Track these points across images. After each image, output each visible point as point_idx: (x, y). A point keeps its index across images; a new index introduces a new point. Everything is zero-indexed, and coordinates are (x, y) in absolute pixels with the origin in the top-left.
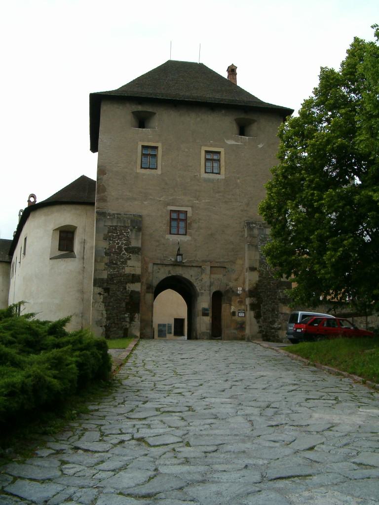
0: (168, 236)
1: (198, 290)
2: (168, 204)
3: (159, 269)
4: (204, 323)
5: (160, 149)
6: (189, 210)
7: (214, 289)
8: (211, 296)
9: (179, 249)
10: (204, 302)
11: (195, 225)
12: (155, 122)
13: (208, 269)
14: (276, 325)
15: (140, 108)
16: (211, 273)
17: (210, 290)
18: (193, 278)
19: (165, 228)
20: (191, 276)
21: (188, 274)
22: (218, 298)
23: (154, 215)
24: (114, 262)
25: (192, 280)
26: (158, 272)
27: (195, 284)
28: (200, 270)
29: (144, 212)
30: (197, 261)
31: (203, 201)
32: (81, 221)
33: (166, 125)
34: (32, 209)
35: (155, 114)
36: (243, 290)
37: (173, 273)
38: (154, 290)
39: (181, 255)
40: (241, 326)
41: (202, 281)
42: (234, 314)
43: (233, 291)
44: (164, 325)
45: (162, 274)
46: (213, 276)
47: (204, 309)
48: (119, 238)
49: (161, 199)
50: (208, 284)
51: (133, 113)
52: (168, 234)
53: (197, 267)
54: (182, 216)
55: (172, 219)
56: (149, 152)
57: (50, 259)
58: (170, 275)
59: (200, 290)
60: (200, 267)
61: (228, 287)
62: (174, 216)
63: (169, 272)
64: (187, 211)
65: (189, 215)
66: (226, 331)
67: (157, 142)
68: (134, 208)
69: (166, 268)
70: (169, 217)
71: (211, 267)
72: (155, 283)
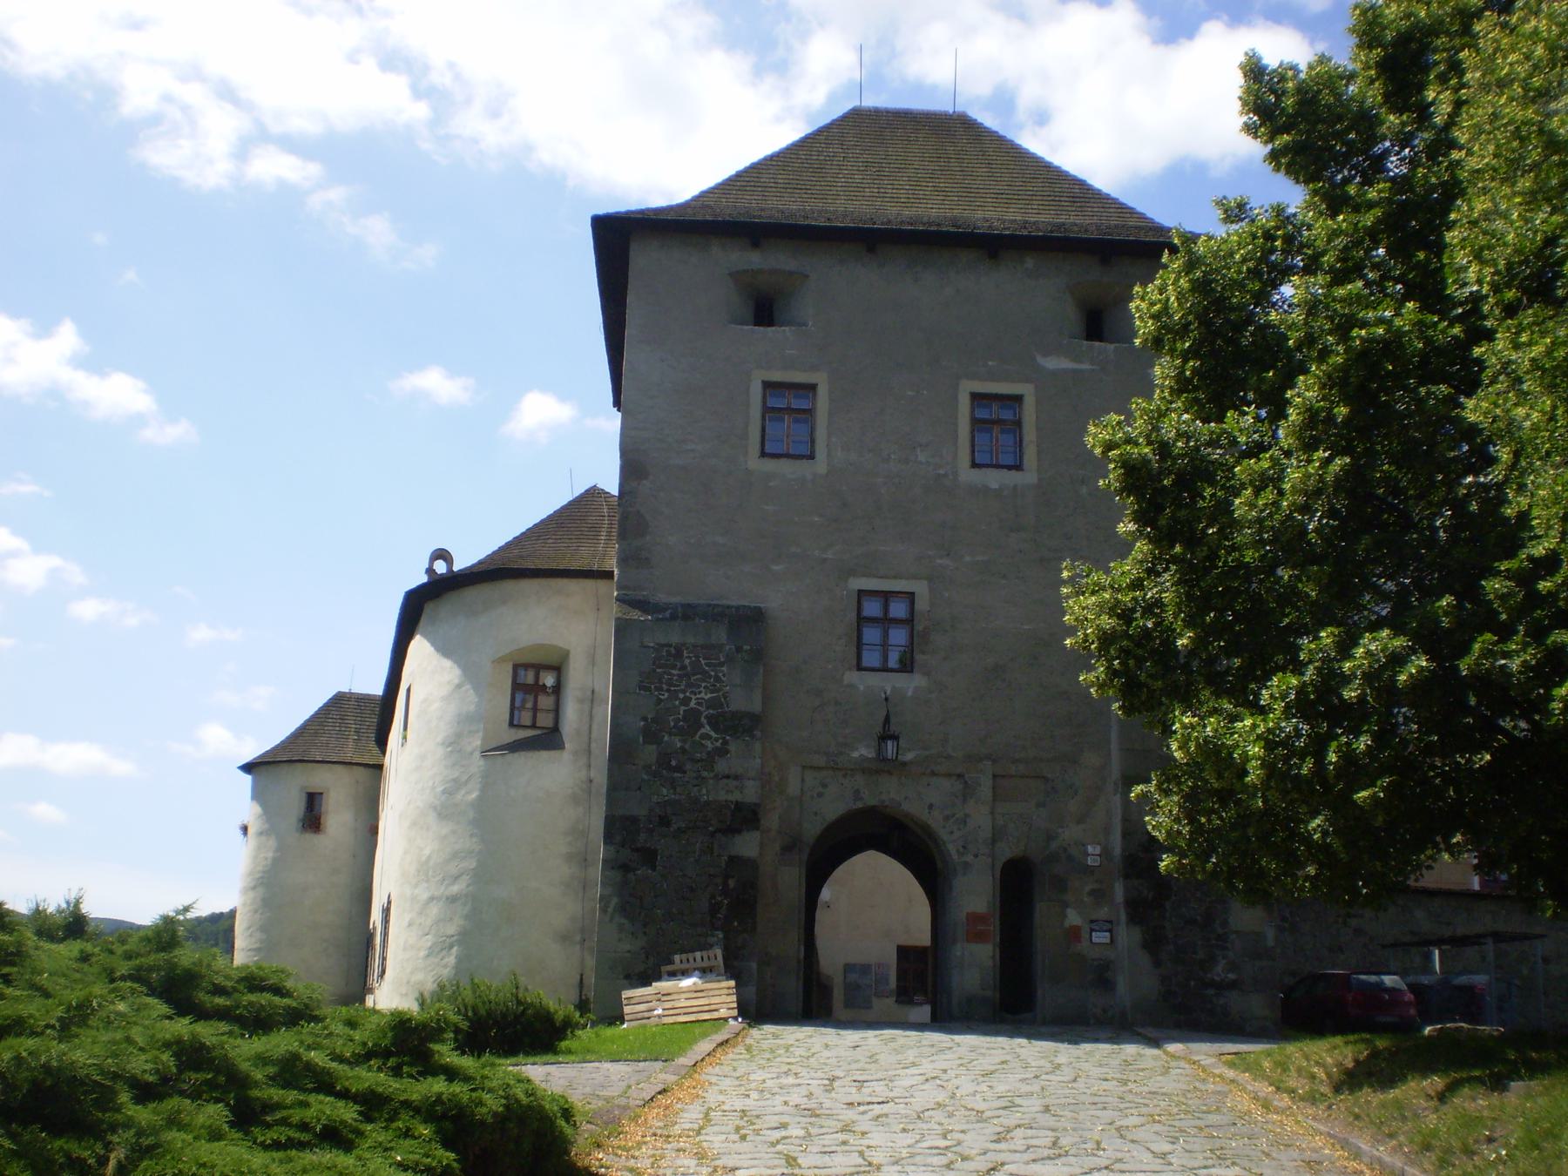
0: (852, 677)
1: (955, 857)
2: (853, 573)
3: (825, 786)
4: (974, 964)
6: (920, 588)
7: (1006, 851)
8: (998, 876)
9: (887, 720)
10: (975, 894)
13: (985, 789)
14: (1219, 971)
15: (754, 259)
21: (919, 800)
22: (1019, 883)
23: (795, 600)
24: (674, 763)
25: (935, 821)
26: (820, 795)
27: (943, 834)
29: (773, 599)
30: (949, 757)
31: (968, 559)
36: (1106, 853)
37: (870, 800)
38: (805, 857)
39: (895, 738)
40: (1102, 976)
42: (1074, 934)
44: (865, 969)
47: (974, 918)
48: (689, 685)
49: (829, 555)
51: (736, 276)
53: (949, 775)
54: (898, 610)
55: (862, 620)
56: (788, 403)
58: (860, 805)
59: (961, 854)
60: (960, 776)
61: (1054, 845)
62: (872, 608)
63: (857, 794)
64: (913, 594)
65: (922, 605)
66: (1047, 995)
68: (733, 586)
70: (854, 614)
71: (994, 776)
72: (812, 829)
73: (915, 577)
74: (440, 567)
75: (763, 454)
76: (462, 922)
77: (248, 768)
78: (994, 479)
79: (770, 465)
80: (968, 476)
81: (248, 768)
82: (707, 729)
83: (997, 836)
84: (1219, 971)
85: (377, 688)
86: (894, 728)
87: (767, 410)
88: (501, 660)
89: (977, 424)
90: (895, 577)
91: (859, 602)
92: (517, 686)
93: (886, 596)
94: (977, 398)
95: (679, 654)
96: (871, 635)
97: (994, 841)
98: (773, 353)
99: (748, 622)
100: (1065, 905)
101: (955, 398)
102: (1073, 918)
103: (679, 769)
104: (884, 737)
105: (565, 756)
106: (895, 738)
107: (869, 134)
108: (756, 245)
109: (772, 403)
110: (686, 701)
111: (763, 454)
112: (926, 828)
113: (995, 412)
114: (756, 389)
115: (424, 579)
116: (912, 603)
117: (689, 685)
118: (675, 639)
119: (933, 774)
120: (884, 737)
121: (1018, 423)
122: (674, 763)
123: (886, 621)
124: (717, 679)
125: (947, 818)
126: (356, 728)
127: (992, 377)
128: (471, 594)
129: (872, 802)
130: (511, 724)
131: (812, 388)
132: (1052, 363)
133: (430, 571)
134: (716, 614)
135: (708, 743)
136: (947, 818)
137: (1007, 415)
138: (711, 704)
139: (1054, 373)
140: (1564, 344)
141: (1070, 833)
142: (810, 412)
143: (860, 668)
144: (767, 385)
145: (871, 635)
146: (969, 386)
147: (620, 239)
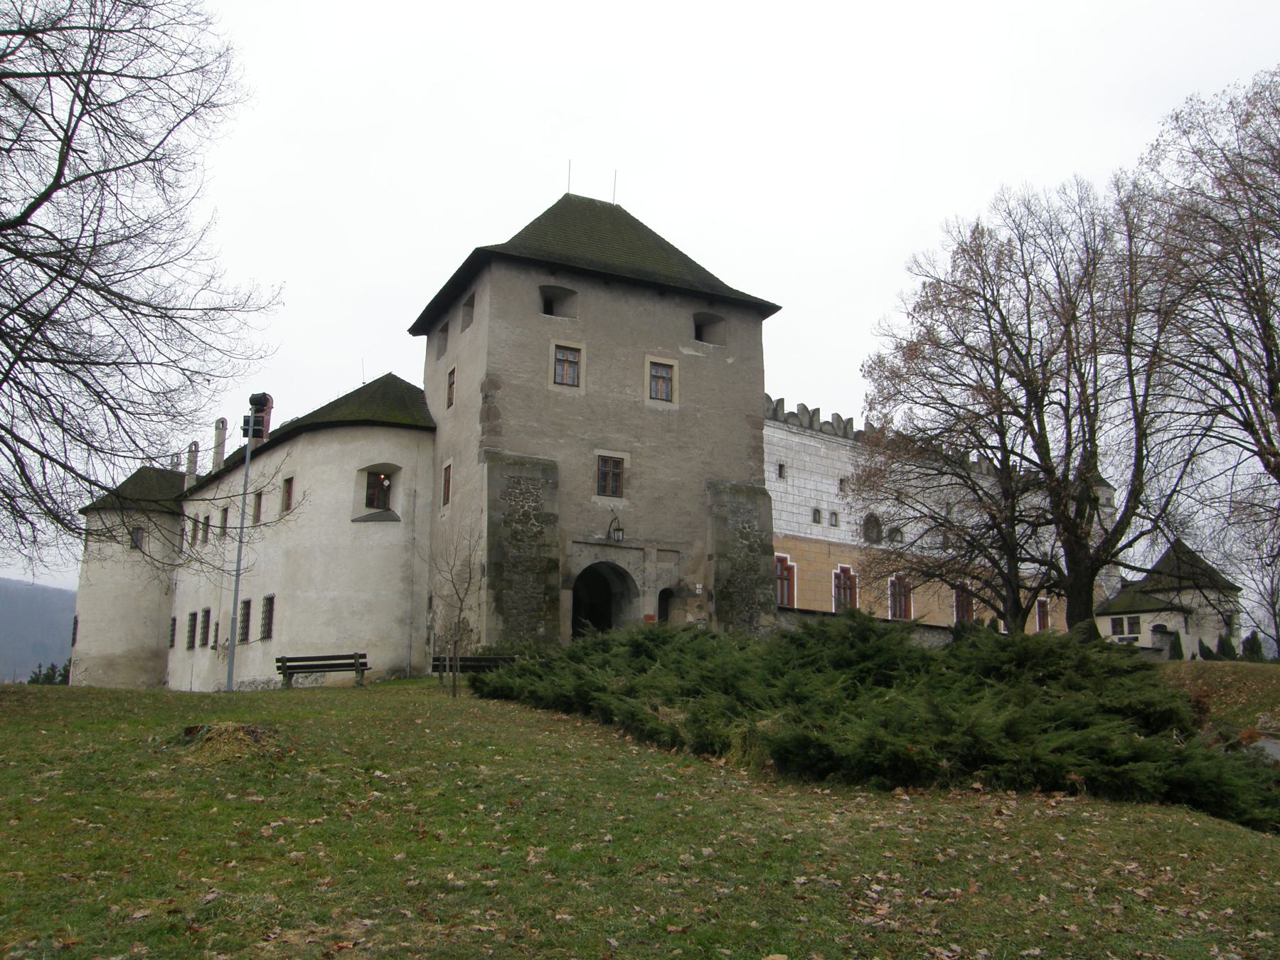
0: (595, 498)
2: (596, 446)
5: (583, 353)
6: (626, 456)
7: (661, 587)
11: (635, 483)
13: (654, 552)
15: (552, 281)
16: (659, 560)
23: (575, 464)
25: (630, 569)
27: (634, 577)
28: (641, 553)
29: (559, 457)
35: (575, 293)
36: (704, 588)
46: (661, 565)
50: (654, 577)
67: (579, 341)
68: (542, 450)
72: (576, 571)
78: (661, 406)
79: (558, 389)
80: (649, 403)
81: (416, 330)
82: (533, 521)
83: (658, 578)
87: (558, 360)
88: (362, 470)
89: (654, 377)
94: (654, 364)
95: (518, 483)
98: (560, 329)
99: (549, 470)
100: (686, 611)
101: (643, 364)
103: (521, 540)
105: (401, 524)
107: (572, 212)
110: (523, 507)
113: (663, 373)
114: (552, 348)
118: (516, 474)
121: (671, 380)
127: (660, 355)
131: (578, 350)
132: (686, 351)
134: (536, 464)
137: (571, 358)
138: (535, 509)
139: (688, 356)
140: (93, 5)
144: (558, 347)
146: (650, 358)
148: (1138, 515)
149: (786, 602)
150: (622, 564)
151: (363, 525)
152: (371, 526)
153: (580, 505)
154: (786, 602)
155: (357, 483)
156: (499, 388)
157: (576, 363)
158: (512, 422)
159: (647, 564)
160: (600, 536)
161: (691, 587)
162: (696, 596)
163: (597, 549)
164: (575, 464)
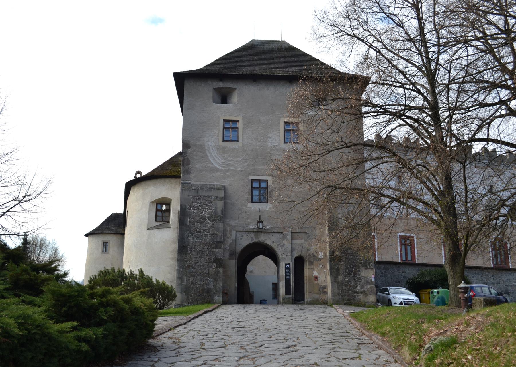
0: (250, 205)
2: (250, 174)
3: (242, 236)
6: (270, 179)
7: (296, 255)
12: (235, 98)
13: (289, 236)
15: (221, 84)
17: (292, 256)
18: (275, 244)
19: (248, 196)
20: (273, 242)
21: (269, 240)
23: (238, 188)
24: (198, 230)
25: (274, 246)
26: (241, 239)
27: (277, 250)
28: (281, 236)
29: (227, 183)
30: (278, 227)
32: (171, 191)
33: (244, 95)
34: (129, 186)
35: (235, 89)
36: (325, 255)
39: (262, 222)
41: (283, 246)
43: (314, 256)
45: (245, 241)
48: (202, 208)
50: (289, 249)
51: (216, 90)
52: (249, 202)
53: (279, 233)
57: (148, 229)
58: (253, 242)
59: (282, 255)
60: (282, 233)
62: (256, 185)
67: (238, 116)
69: (248, 235)
70: (250, 187)
72: (239, 249)
73: (269, 175)
74: (138, 176)
75: (224, 141)
76: (170, 286)
77: (87, 235)
79: (225, 144)
81: (87, 235)
84: (358, 288)
85: (122, 212)
86: (262, 219)
87: (224, 128)
88: (153, 202)
90: (262, 175)
91: (252, 183)
92: (157, 210)
93: (260, 181)
95: (199, 199)
96: (256, 192)
97: (292, 251)
100: (313, 269)
101: (279, 123)
102: (315, 274)
104: (260, 221)
106: (262, 222)
108: (221, 80)
109: (226, 126)
111: (224, 141)
112: (272, 248)
113: (231, 125)
114: (221, 122)
115: (133, 178)
116: (267, 183)
117: (202, 208)
119: (274, 232)
120: (260, 221)
122: (198, 230)
123: (260, 188)
124: (211, 206)
125: (278, 245)
126: (115, 225)
128: (143, 184)
129: (256, 241)
130: (156, 221)
131: (238, 121)
133: (135, 177)
135: (208, 224)
136: (278, 245)
141: (314, 248)
142: (237, 128)
143: (252, 202)
144: (224, 120)
145: (256, 192)
147: (182, 79)
148: (429, 47)
149: (409, 259)
150: (269, 242)
151: (152, 231)
152: (156, 231)
153: (240, 209)
154: (409, 259)
155: (150, 210)
156: (190, 148)
157: (237, 128)
158: (197, 166)
159: (285, 242)
160: (252, 226)
161: (315, 254)
162: (320, 260)
163: (252, 235)
164: (238, 188)
